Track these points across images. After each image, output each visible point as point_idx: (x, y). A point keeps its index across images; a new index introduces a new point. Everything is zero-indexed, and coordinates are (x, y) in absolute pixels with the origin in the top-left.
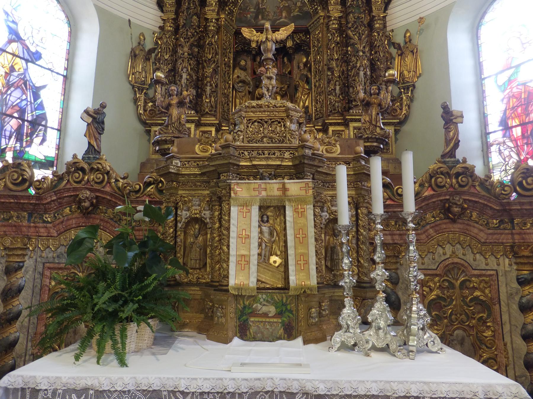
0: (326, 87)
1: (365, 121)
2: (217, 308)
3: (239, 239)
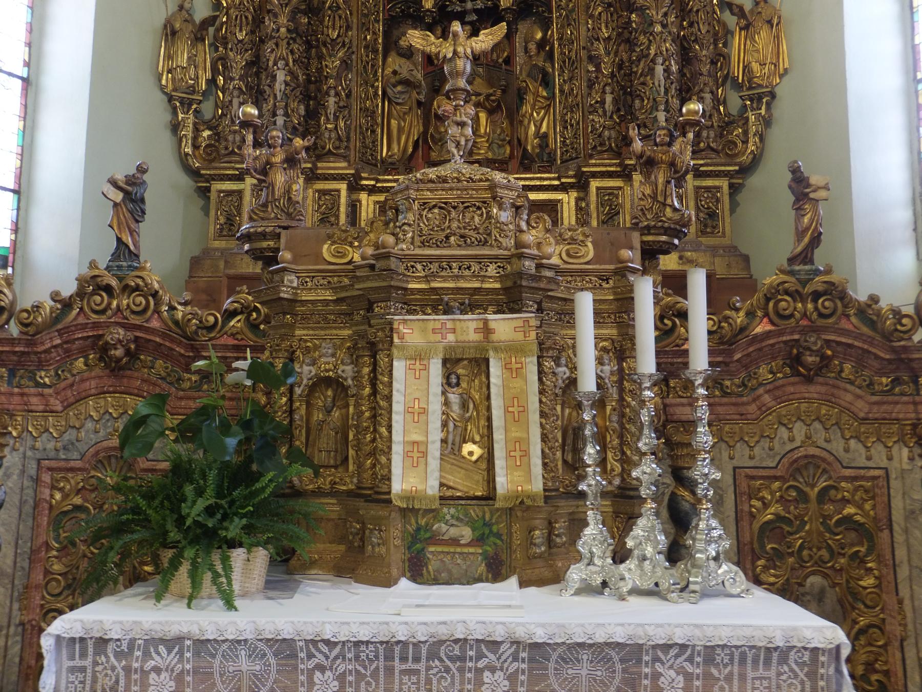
0: (585, 95)
1: (644, 195)
2: (371, 530)
3: (407, 415)
